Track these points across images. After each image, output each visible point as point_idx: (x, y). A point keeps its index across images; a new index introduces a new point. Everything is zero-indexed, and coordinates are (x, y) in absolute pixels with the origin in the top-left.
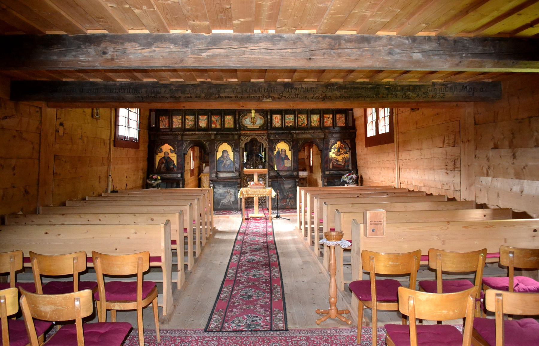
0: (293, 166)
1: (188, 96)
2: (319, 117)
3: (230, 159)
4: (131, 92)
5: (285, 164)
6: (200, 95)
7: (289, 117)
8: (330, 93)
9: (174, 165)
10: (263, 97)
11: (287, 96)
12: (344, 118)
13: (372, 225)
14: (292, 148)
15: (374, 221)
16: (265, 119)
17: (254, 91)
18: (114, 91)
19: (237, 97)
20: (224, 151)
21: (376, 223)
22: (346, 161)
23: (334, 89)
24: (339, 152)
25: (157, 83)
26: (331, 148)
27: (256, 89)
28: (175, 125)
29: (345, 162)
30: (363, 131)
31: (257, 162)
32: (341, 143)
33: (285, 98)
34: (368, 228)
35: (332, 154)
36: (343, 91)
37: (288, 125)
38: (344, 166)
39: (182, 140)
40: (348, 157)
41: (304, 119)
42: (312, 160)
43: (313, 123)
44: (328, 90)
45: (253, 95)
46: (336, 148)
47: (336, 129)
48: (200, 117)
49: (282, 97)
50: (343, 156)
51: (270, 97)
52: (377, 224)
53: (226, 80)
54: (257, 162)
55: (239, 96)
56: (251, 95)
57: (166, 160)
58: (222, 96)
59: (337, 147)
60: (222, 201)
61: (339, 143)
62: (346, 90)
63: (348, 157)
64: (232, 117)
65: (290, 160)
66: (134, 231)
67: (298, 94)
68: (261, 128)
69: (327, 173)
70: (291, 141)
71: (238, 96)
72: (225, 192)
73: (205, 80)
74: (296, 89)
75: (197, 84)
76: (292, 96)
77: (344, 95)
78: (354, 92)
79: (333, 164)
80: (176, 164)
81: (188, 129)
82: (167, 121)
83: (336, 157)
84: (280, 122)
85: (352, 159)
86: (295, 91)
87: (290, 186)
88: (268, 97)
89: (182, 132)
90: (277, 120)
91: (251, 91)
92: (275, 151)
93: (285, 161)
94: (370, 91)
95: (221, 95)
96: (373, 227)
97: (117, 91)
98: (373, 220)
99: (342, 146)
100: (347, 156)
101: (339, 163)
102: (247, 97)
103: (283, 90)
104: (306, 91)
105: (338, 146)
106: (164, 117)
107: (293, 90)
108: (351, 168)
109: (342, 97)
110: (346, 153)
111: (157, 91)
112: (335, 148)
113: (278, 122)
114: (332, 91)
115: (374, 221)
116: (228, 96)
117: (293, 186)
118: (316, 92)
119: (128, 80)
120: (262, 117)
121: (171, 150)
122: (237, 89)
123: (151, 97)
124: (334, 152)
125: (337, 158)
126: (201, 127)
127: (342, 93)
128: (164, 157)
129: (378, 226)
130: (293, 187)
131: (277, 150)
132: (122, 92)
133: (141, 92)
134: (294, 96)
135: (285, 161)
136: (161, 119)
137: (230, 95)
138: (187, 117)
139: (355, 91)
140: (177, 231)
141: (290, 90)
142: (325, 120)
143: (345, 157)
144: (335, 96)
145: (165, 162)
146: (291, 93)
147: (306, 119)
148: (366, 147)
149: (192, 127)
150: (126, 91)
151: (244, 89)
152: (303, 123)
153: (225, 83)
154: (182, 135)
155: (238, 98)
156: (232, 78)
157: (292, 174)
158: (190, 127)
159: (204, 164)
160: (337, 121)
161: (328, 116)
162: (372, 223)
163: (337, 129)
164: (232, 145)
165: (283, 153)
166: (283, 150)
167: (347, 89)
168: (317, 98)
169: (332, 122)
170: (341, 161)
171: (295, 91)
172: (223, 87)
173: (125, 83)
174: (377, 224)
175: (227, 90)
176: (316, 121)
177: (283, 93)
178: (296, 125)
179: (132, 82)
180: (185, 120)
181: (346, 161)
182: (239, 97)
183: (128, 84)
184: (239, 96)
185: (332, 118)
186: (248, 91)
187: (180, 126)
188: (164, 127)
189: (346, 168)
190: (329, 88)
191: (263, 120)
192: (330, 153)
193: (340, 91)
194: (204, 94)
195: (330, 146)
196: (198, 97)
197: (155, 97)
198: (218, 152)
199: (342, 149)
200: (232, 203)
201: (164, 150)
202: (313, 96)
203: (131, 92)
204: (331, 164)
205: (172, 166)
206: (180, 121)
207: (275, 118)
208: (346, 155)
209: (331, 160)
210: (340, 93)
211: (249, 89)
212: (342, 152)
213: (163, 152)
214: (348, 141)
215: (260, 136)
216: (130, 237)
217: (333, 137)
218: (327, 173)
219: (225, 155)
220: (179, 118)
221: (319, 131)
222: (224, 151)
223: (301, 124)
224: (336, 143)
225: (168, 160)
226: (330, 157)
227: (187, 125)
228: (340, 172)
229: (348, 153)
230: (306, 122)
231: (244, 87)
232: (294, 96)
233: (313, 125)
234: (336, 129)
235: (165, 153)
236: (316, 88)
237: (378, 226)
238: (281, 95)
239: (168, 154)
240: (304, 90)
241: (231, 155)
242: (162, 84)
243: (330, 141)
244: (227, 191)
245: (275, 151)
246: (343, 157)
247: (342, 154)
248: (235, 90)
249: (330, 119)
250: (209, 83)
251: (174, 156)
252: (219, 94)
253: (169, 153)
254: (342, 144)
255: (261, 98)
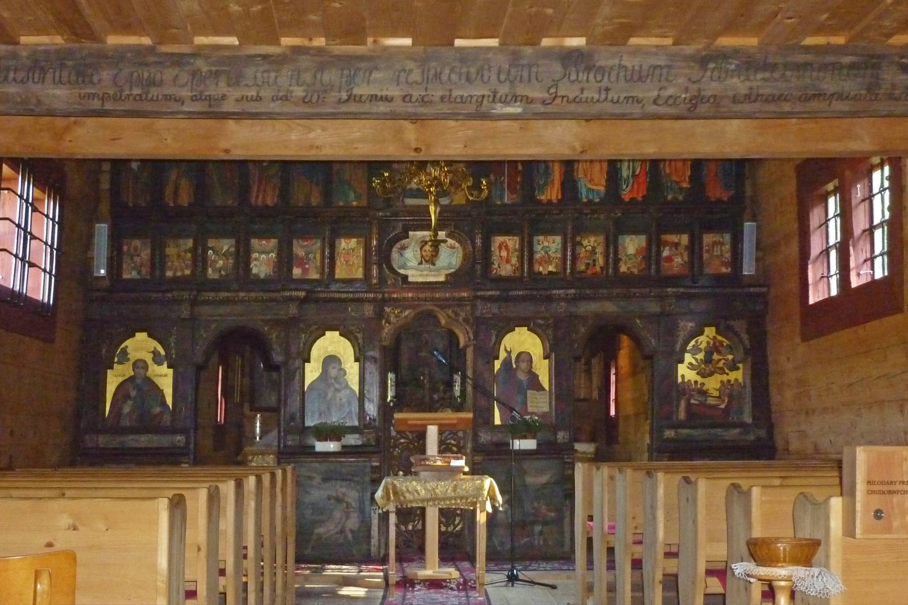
0: (556, 410)
1: (250, 94)
2: (644, 244)
3: (347, 386)
4: (65, 79)
5: (529, 404)
6: (287, 91)
7: (546, 244)
8: (714, 85)
9: (164, 403)
10: (494, 96)
11: (572, 96)
12: (728, 247)
13: (876, 497)
14: (552, 350)
15: (882, 483)
16: (464, 249)
17: (464, 78)
18: (11, 75)
19: (407, 99)
20: (331, 360)
21: (886, 488)
22: (730, 391)
23: (727, 71)
24: (707, 368)
25: (151, 50)
26: (684, 350)
27: (473, 70)
28: (171, 268)
29: (730, 396)
30: (793, 285)
31: (435, 397)
32: (717, 332)
33: (565, 103)
34: (859, 506)
35: (685, 372)
36: (760, 76)
37: (541, 269)
38: (727, 411)
39: (193, 318)
40: (741, 380)
41: (594, 248)
42: (616, 400)
43: (626, 263)
44: (708, 73)
45: (461, 93)
46: (700, 350)
47: (700, 283)
48: (254, 242)
49: (554, 99)
50: (725, 378)
51: (516, 98)
52: (890, 492)
53: (375, 42)
54: (435, 397)
55: (416, 94)
56: (456, 93)
57: (139, 389)
58: (361, 96)
59: (703, 346)
60: (317, 531)
61: (710, 331)
62: (767, 75)
63: (741, 380)
64: (358, 243)
65: (544, 389)
66: (70, 521)
67: (607, 90)
68: (455, 279)
69: (669, 433)
70: (548, 326)
71: (411, 96)
72: (329, 498)
73: (306, 43)
74: (601, 69)
75: (279, 55)
76: (590, 95)
77: (761, 91)
78: (793, 79)
79: (689, 405)
80: (169, 401)
81: (214, 281)
82: (146, 254)
83: (699, 379)
84: (514, 260)
85: (754, 388)
86: (599, 78)
87: (543, 479)
88: (509, 98)
89: (195, 293)
90: (504, 254)
91: (454, 77)
92: (497, 358)
93: (530, 393)
94: (848, 75)
95: (357, 91)
96: (877, 502)
97: (21, 75)
98: (876, 478)
99: (721, 342)
100: (737, 376)
101: (711, 401)
102: (442, 98)
103: (558, 76)
104: (636, 78)
105: (708, 343)
106: (137, 243)
107: (591, 76)
108: (748, 419)
109: (753, 98)
110: (734, 368)
111: (149, 77)
112: (696, 350)
113: (508, 261)
114: (723, 76)
115: (882, 483)
116: (379, 94)
117: (553, 480)
118: (667, 80)
119: (59, 40)
120: (457, 245)
121: (155, 353)
122: (411, 71)
123: (129, 96)
124: (694, 362)
125: (703, 384)
126: (257, 275)
127: (754, 84)
128: (131, 379)
129: (895, 500)
130: (556, 483)
131: (503, 355)
132: (36, 80)
133: (100, 81)
134: (596, 96)
135: (530, 393)
136: (125, 248)
137: (384, 93)
138: (211, 243)
139: (798, 77)
140: (199, 549)
141: (583, 76)
142: (666, 253)
143: (729, 381)
144: (730, 93)
145: (133, 393)
146: (585, 85)
147: (600, 250)
148: (805, 338)
149: (227, 275)
150: (49, 76)
151: (432, 72)
152: (591, 262)
153: (370, 50)
154: (194, 303)
155: (410, 101)
156: (394, 35)
157: (552, 438)
158: (221, 276)
159: (258, 416)
160: (706, 256)
161: (672, 238)
162: (876, 488)
163: (702, 282)
164: (356, 338)
165: (523, 365)
166: (525, 357)
167: (773, 71)
168: (671, 101)
169: (686, 259)
170: (717, 394)
171: (599, 78)
172: (363, 65)
173: (45, 52)
174: (890, 492)
175: (377, 75)
176: (635, 255)
177: (560, 84)
178: (568, 271)
179: (69, 45)
180: (205, 251)
181: (735, 393)
182: (414, 99)
183: (58, 52)
184: (416, 94)
185: (686, 248)
186: (444, 78)
187: (187, 272)
188: (134, 275)
189: (733, 418)
190: (711, 65)
191: (461, 255)
192: (680, 366)
193: (748, 79)
194: (301, 88)
195: (680, 341)
196: (281, 99)
197: (144, 97)
198: (308, 361)
199: (719, 353)
200: (350, 536)
201: (133, 355)
202: (659, 96)
203: (65, 79)
204: (683, 404)
205: (158, 410)
206: (189, 255)
207: (500, 248)
208: (734, 372)
209: (685, 390)
210: (748, 84)
211: (447, 71)
212: (721, 364)
213: (128, 360)
214: (740, 326)
215: (449, 307)
216: (54, 543)
217: (691, 312)
218: (669, 433)
219: (333, 372)
220: (186, 244)
221: (643, 291)
222: (331, 360)
223: (583, 267)
224: (701, 333)
225: (146, 388)
226: (680, 380)
227: (210, 271)
228: (713, 431)
229: (741, 365)
230: (601, 261)
231: (433, 64)
232: (596, 96)
233: (623, 269)
234: (700, 283)
235: (135, 365)
236: (669, 67)
237: (896, 499)
238: (553, 90)
239: (146, 367)
240: (629, 73)
241: (352, 369)
242: (167, 54)
243: (682, 324)
244: (334, 494)
245: (497, 358)
246: (722, 382)
247: (721, 369)
248: (402, 74)
249: (680, 248)
250: (320, 51)
251: (166, 375)
252: (352, 89)
253: (150, 361)
254: (720, 338)
255: (485, 102)
